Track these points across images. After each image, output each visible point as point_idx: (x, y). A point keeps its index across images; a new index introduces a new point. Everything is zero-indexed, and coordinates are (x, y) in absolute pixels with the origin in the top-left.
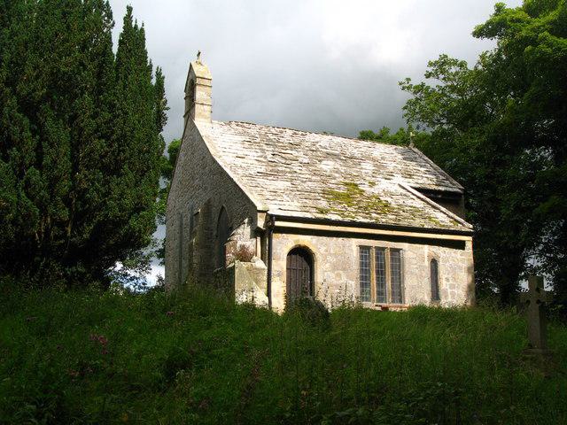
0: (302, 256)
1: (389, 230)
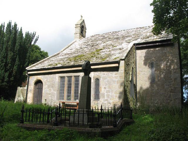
0: (39, 83)
1: (45, 70)
